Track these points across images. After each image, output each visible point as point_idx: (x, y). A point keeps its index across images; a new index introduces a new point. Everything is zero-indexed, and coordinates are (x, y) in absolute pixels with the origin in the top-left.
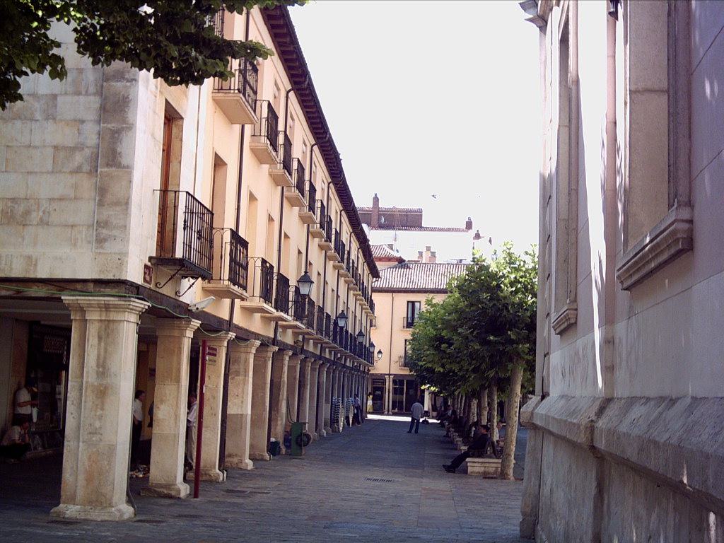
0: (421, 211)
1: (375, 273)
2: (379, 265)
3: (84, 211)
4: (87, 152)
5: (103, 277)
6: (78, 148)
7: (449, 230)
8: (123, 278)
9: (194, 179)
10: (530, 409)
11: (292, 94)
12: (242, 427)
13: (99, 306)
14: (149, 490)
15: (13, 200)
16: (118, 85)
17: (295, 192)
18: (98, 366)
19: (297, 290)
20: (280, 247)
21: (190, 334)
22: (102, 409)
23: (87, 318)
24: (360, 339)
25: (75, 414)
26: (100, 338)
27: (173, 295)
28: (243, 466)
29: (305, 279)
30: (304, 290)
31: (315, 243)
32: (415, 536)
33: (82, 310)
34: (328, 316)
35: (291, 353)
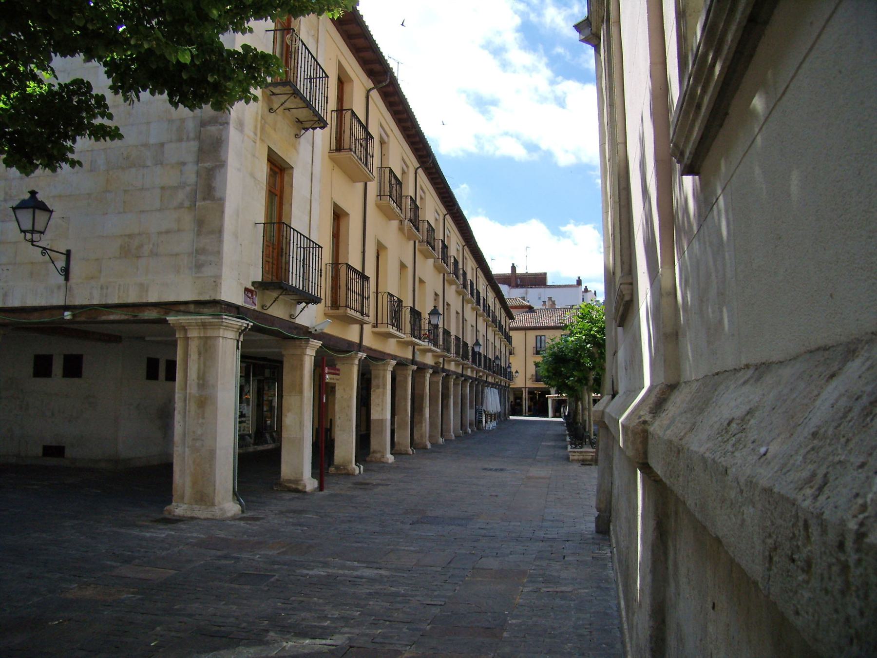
0: (545, 274)
1: (511, 317)
2: (513, 311)
3: (185, 242)
4: (188, 189)
5: (202, 298)
6: (182, 186)
7: (565, 286)
8: (218, 298)
9: (308, 218)
10: (601, 408)
11: (420, 171)
12: (382, 432)
13: (197, 325)
14: (280, 485)
15: (130, 236)
16: (212, 129)
17: (453, 276)
18: (198, 378)
19: (473, 349)
20: (414, 291)
21: (390, 369)
22: (203, 418)
23: (189, 336)
24: (497, 362)
25: (182, 423)
26: (200, 354)
27: (286, 317)
28: (384, 460)
29: (477, 343)
30: (477, 349)
31: (468, 307)
32: (491, 534)
33: (184, 329)
34: (490, 359)
35: (431, 371)
